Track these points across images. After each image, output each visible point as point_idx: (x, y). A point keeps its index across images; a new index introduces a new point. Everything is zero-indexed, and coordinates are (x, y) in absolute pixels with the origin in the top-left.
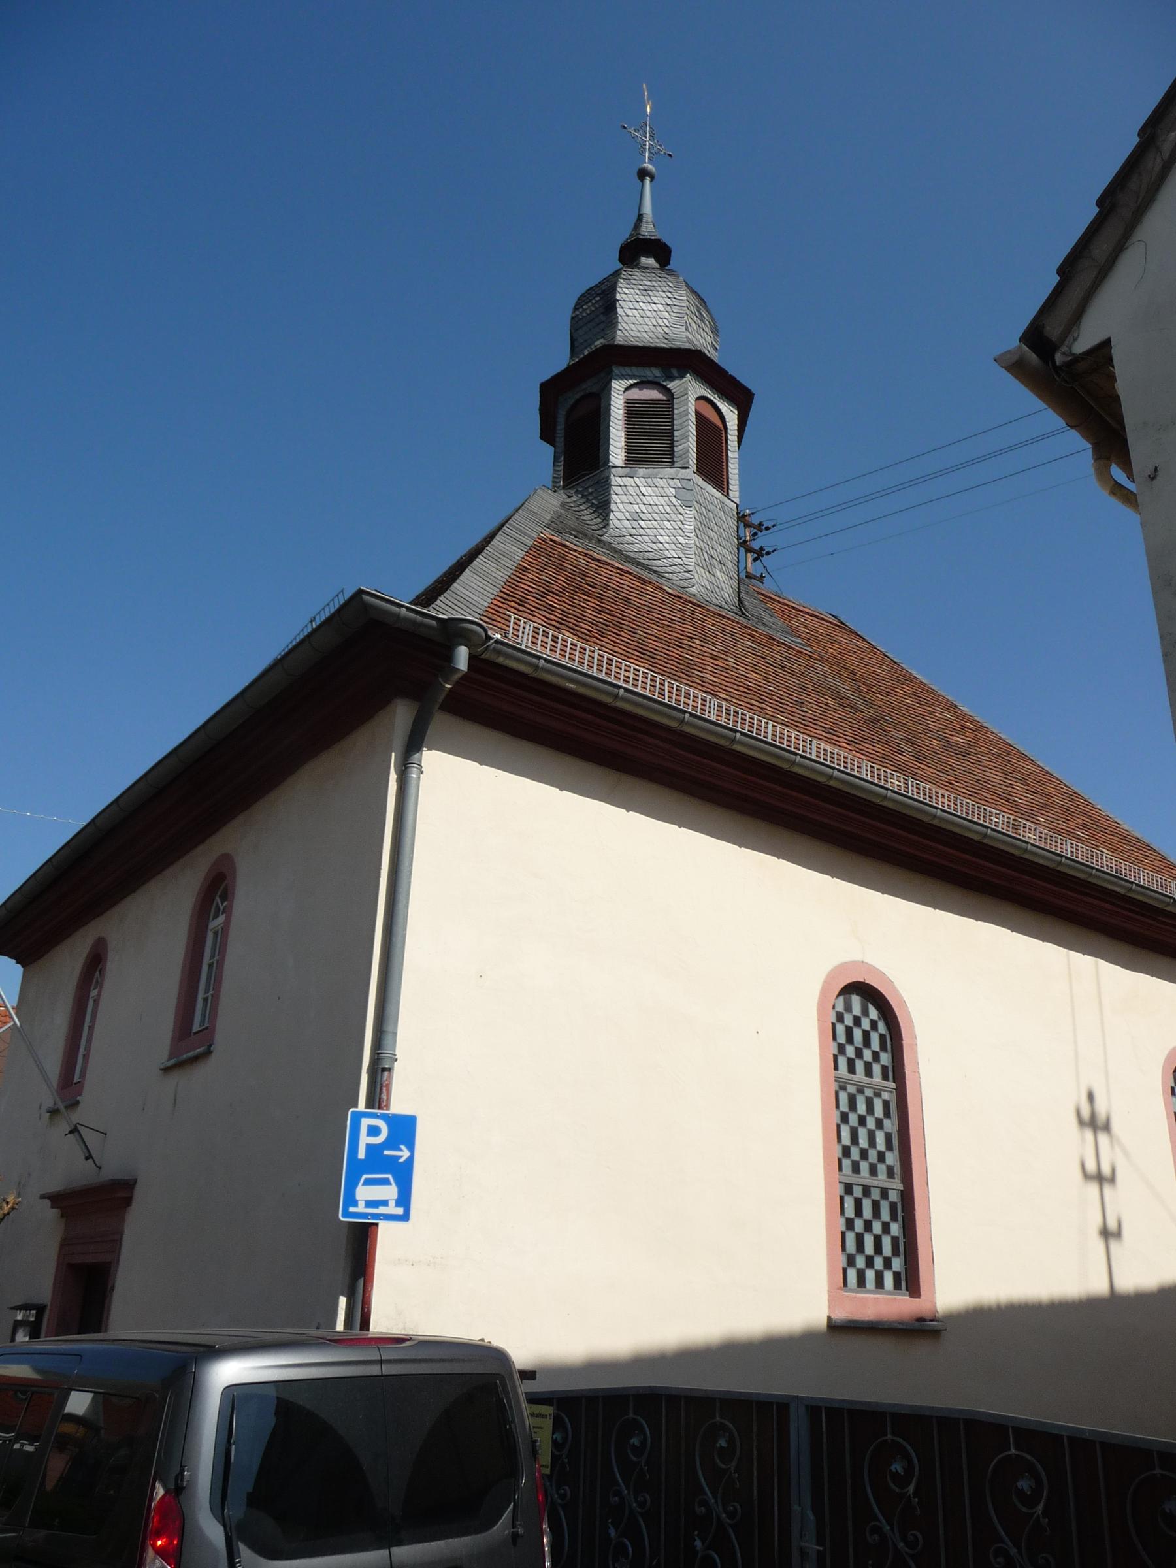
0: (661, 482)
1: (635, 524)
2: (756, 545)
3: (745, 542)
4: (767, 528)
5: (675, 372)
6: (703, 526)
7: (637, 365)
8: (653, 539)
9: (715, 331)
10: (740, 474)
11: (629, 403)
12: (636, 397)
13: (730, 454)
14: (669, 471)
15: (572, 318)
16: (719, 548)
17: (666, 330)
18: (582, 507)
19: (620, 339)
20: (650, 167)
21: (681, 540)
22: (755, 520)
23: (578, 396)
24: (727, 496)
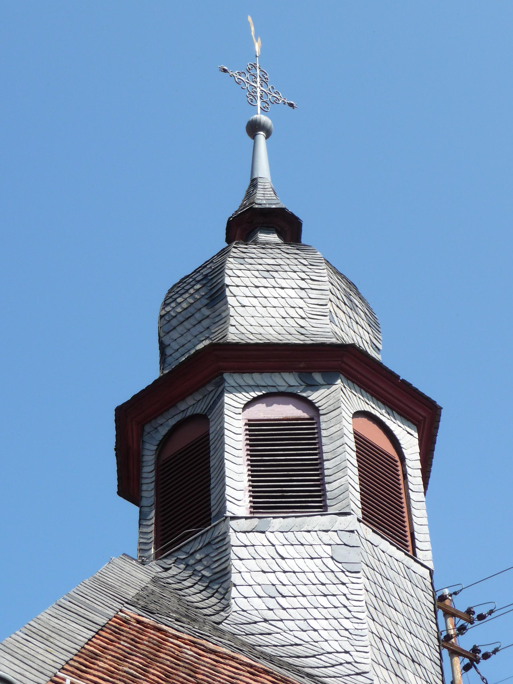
0: (309, 538)
1: (272, 603)
2: (465, 642)
3: (448, 637)
4: (481, 617)
5: (318, 377)
6: (381, 601)
7: (261, 370)
8: (303, 625)
9: (374, 324)
10: (431, 525)
11: (254, 427)
12: (261, 416)
13: (412, 495)
14: (318, 521)
15: (161, 317)
16: (409, 638)
17: (302, 322)
18: (187, 583)
19: (233, 335)
20: (264, 118)
21: (347, 624)
22: (460, 604)
23: (172, 422)
24: (414, 556)
